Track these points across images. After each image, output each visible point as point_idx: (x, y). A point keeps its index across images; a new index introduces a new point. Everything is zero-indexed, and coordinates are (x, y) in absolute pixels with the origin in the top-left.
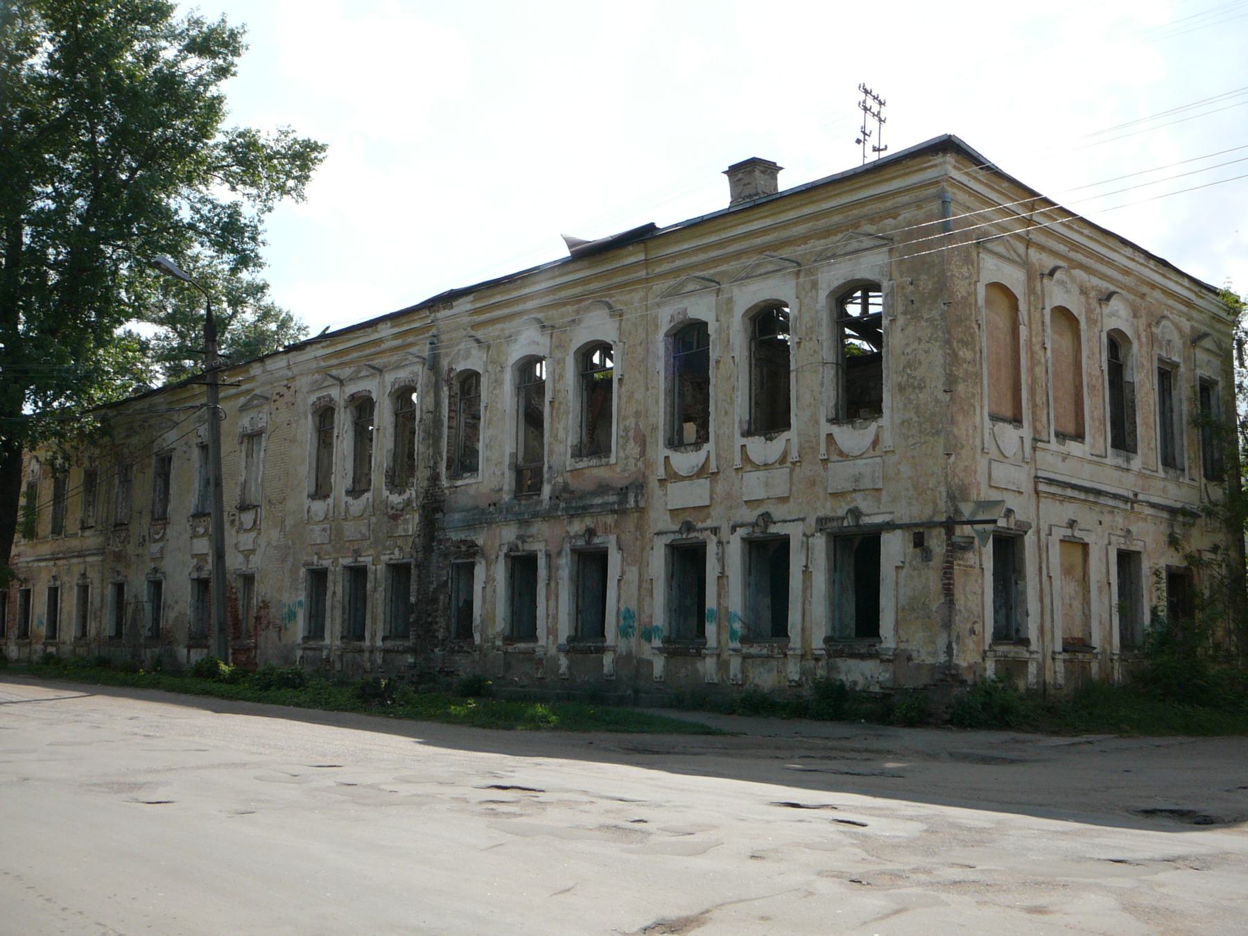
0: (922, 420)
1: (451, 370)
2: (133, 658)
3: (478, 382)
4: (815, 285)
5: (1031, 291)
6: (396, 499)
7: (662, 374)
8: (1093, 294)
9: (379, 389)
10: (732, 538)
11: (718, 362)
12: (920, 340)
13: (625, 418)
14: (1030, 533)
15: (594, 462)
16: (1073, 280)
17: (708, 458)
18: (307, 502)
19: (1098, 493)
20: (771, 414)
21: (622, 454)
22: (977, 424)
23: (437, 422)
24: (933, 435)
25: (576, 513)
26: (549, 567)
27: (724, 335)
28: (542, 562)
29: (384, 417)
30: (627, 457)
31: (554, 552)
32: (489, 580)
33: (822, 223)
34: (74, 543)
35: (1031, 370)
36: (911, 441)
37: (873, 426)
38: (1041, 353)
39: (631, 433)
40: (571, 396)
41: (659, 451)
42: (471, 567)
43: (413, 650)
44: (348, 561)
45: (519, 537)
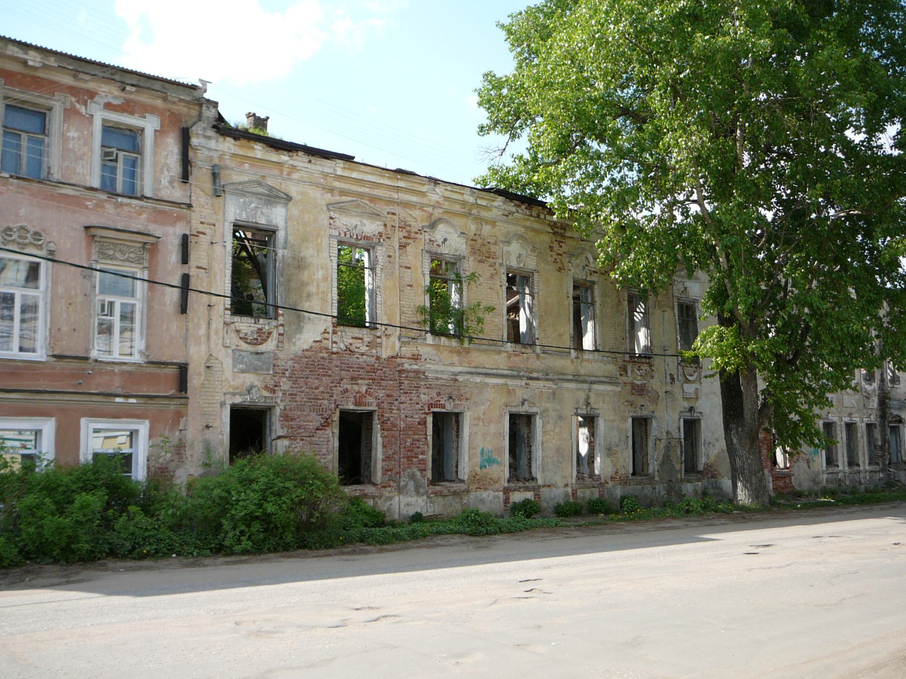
2: (669, 493)
43: (882, 470)
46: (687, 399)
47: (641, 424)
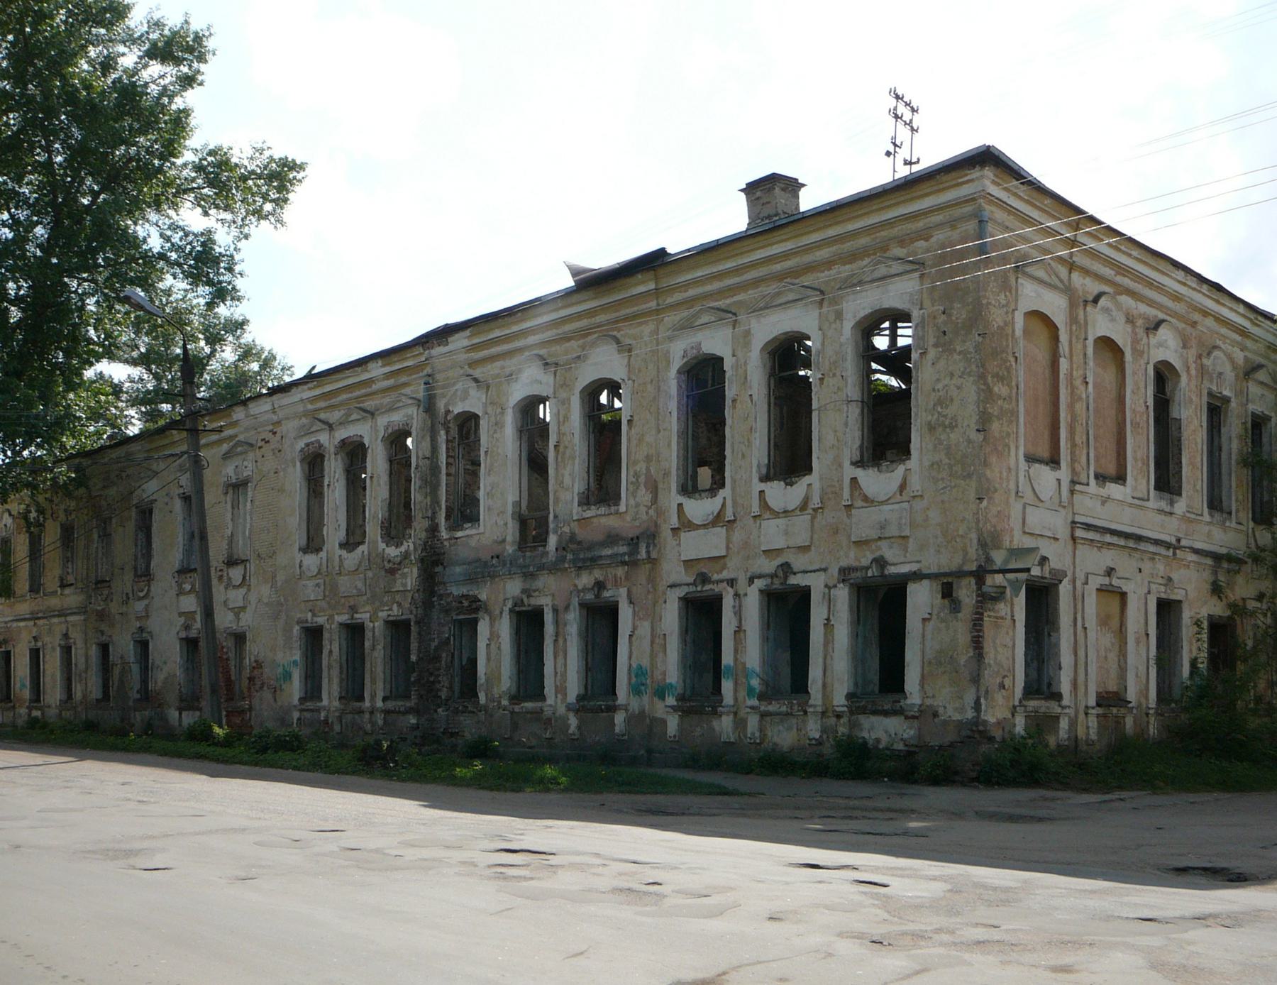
1: (448, 412)
2: (122, 720)
4: (839, 316)
6: (392, 552)
7: (675, 414)
8: (1140, 322)
9: (371, 433)
11: (734, 401)
12: (952, 375)
13: (635, 463)
14: (1065, 581)
15: (603, 510)
17: (724, 505)
18: (299, 556)
19: (1139, 538)
21: (632, 502)
23: (435, 469)
24: (964, 478)
26: (557, 623)
28: (548, 617)
30: (637, 505)
31: (561, 608)
32: (494, 636)
34: (54, 602)
35: (1071, 406)
36: (941, 485)
38: (1082, 388)
40: (577, 439)
41: (671, 498)
42: (474, 623)
43: (415, 711)
44: (344, 618)
45: (524, 591)
46: (138, 618)
47: (104, 648)
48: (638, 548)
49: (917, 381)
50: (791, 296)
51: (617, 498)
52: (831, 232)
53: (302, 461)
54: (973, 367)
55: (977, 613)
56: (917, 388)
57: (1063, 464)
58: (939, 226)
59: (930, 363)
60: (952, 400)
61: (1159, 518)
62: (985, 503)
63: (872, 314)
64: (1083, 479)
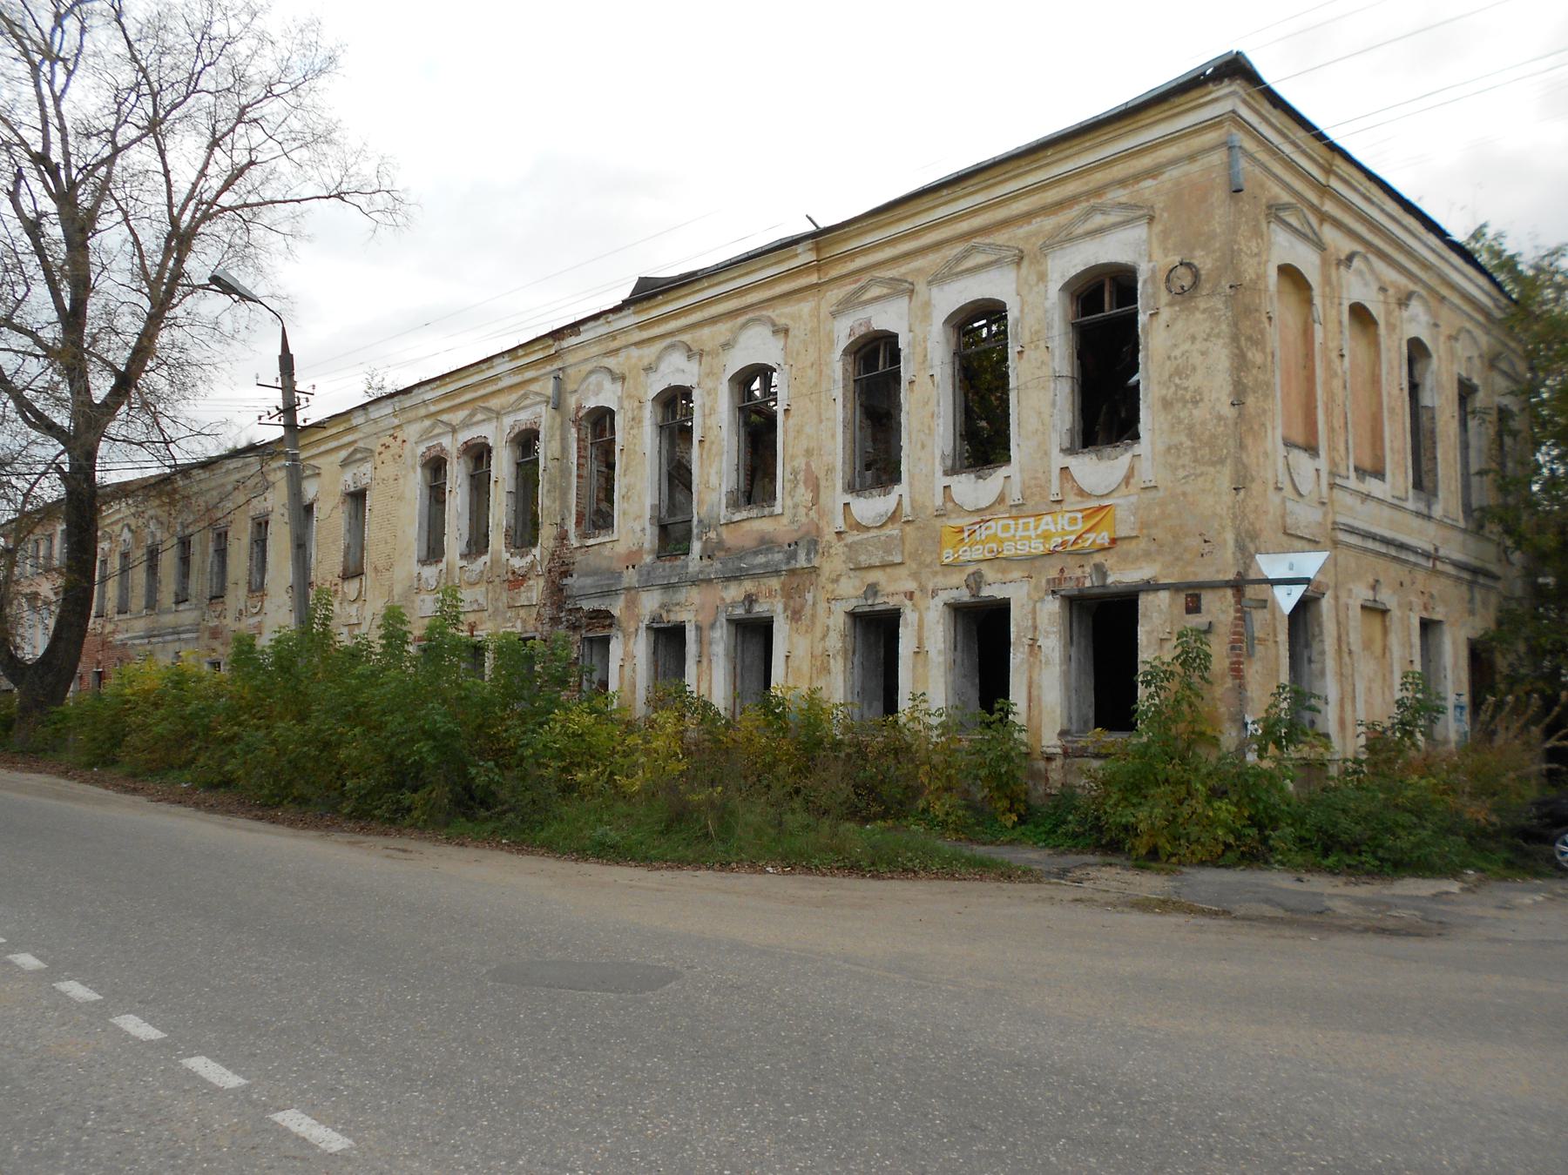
0: (1197, 445)
1: (579, 408)
3: (612, 419)
4: (1042, 277)
5: (1327, 280)
6: (518, 563)
7: (840, 400)
8: (1391, 291)
9: (497, 435)
10: (932, 603)
11: (912, 382)
12: (1193, 338)
13: (793, 457)
14: (1329, 595)
15: (754, 513)
16: (1372, 270)
17: (899, 504)
18: (416, 568)
19: (1402, 546)
20: (983, 439)
21: (789, 502)
22: (1270, 451)
23: (565, 472)
24: (1213, 464)
25: (735, 577)
26: (700, 641)
27: (918, 349)
28: (691, 635)
29: (502, 466)
30: (796, 506)
31: (706, 625)
32: (628, 657)
33: (1052, 196)
34: (168, 620)
35: (1327, 383)
36: (1181, 473)
37: (1125, 459)
38: (1337, 361)
39: (801, 477)
40: (725, 433)
41: (835, 495)
42: (606, 641)
45: (663, 606)
48: (795, 564)
49: (1146, 348)
50: (980, 259)
51: (772, 496)
52: (1030, 179)
53: (424, 466)
54: (1224, 327)
55: (1235, 633)
56: (1147, 356)
57: (1322, 453)
58: (1174, 162)
59: (1163, 325)
60: (1194, 369)
61: (1417, 523)
62: (1242, 492)
63: (1084, 272)
64: (1343, 472)
